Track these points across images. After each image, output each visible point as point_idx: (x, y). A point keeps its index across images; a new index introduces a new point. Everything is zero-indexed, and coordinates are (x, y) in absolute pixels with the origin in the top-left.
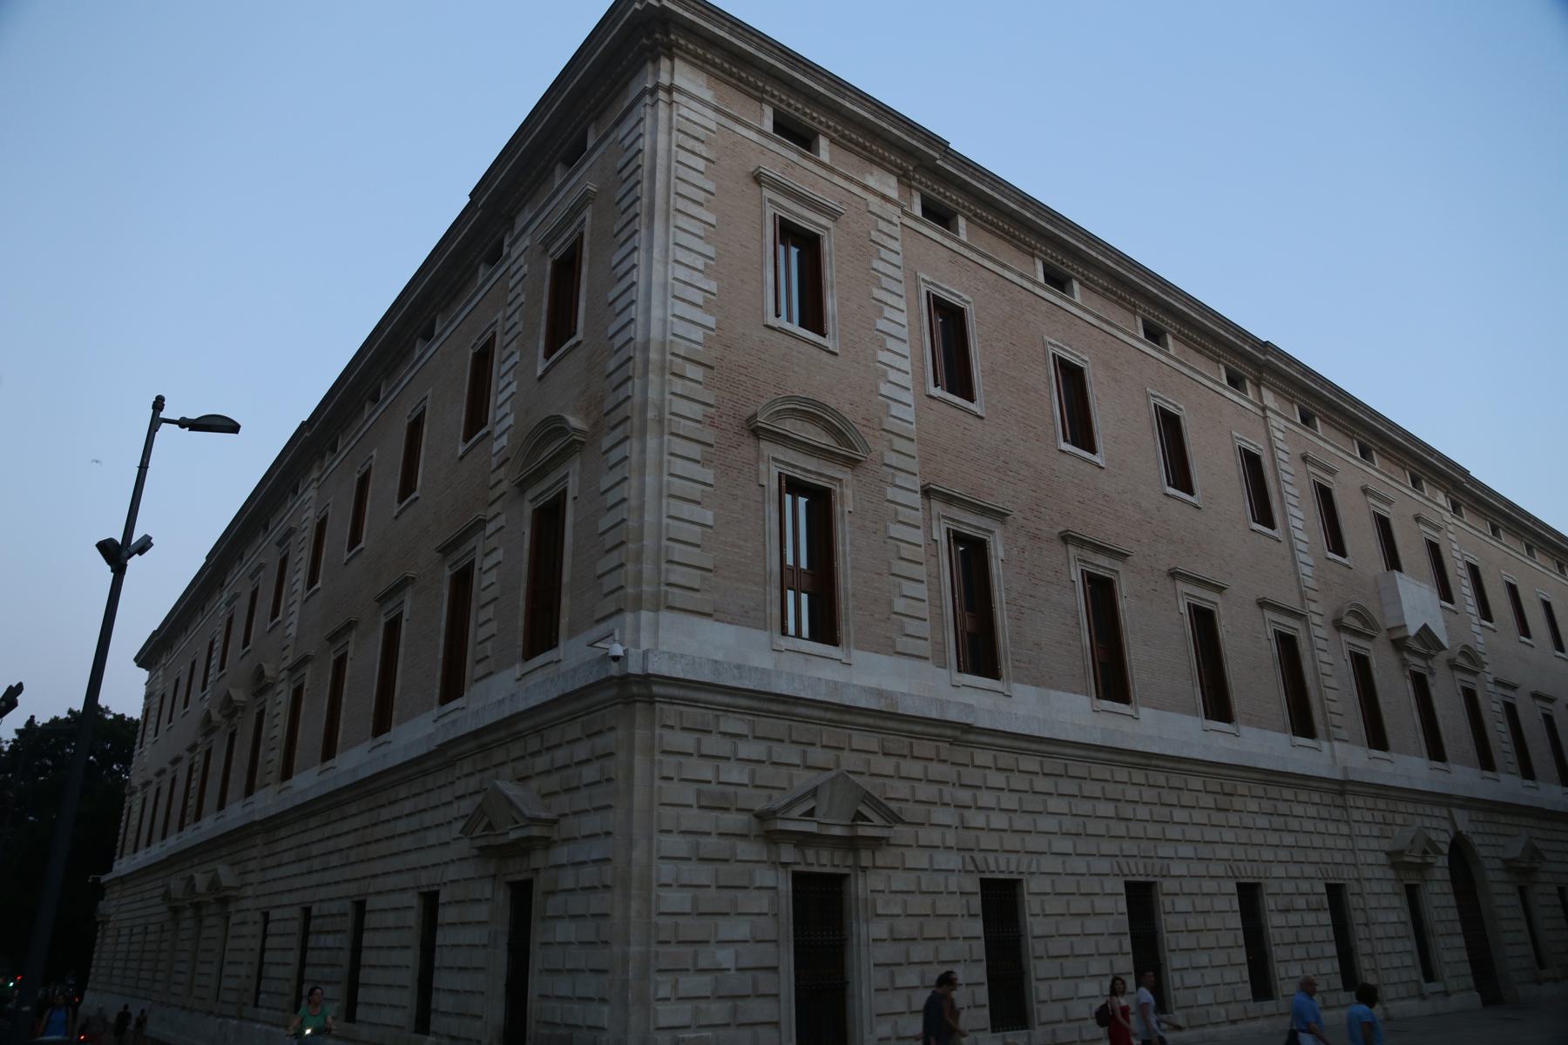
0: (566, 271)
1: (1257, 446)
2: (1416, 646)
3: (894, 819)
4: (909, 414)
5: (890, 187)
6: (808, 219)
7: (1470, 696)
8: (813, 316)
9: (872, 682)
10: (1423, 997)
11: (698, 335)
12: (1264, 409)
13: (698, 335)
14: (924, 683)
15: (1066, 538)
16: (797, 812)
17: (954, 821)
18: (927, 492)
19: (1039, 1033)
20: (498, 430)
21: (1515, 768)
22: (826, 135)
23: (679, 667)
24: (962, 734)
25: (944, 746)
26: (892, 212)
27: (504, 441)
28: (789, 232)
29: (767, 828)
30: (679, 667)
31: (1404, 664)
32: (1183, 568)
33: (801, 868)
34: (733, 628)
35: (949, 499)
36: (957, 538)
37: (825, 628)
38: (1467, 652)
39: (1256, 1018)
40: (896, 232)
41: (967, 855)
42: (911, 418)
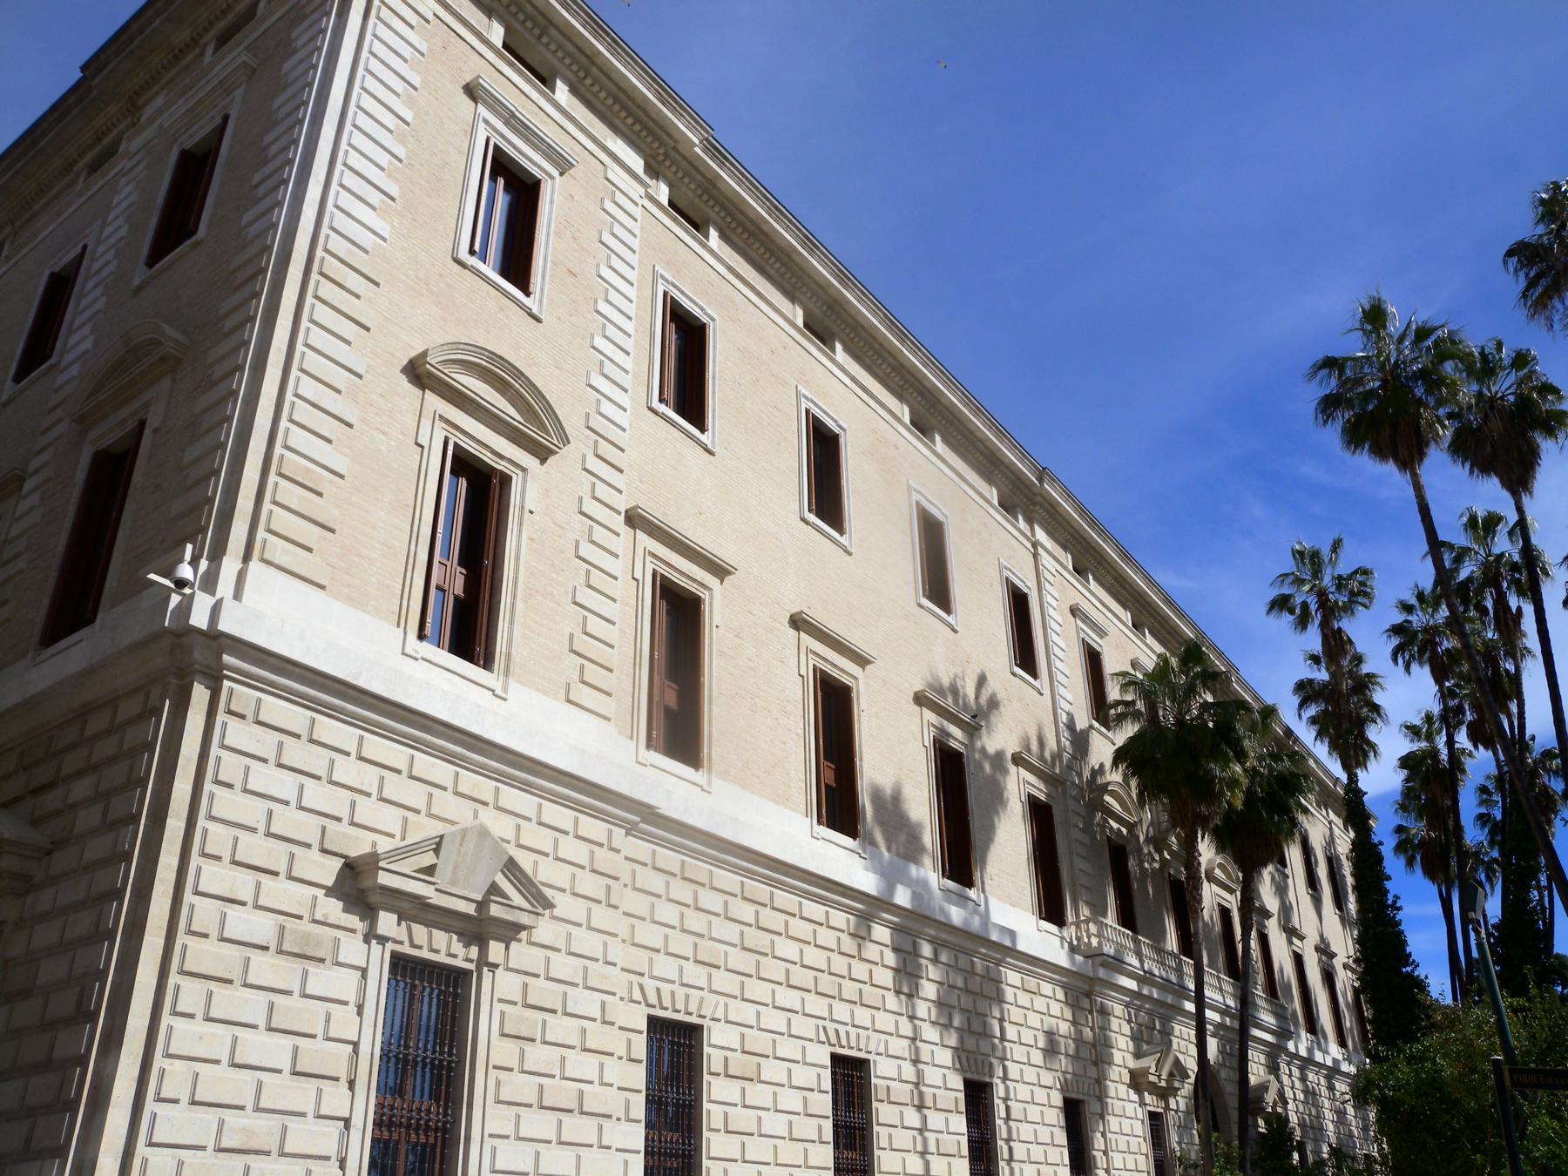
0: (194, 170)
1: (1028, 584)
6: (531, 160)
12: (1035, 545)
14: (600, 738)
16: (406, 866)
17: (624, 933)
20: (69, 358)
24: (644, 818)
25: (619, 833)
26: (636, 190)
27: (74, 371)
28: (502, 166)
29: (357, 886)
33: (407, 949)
40: (637, 212)
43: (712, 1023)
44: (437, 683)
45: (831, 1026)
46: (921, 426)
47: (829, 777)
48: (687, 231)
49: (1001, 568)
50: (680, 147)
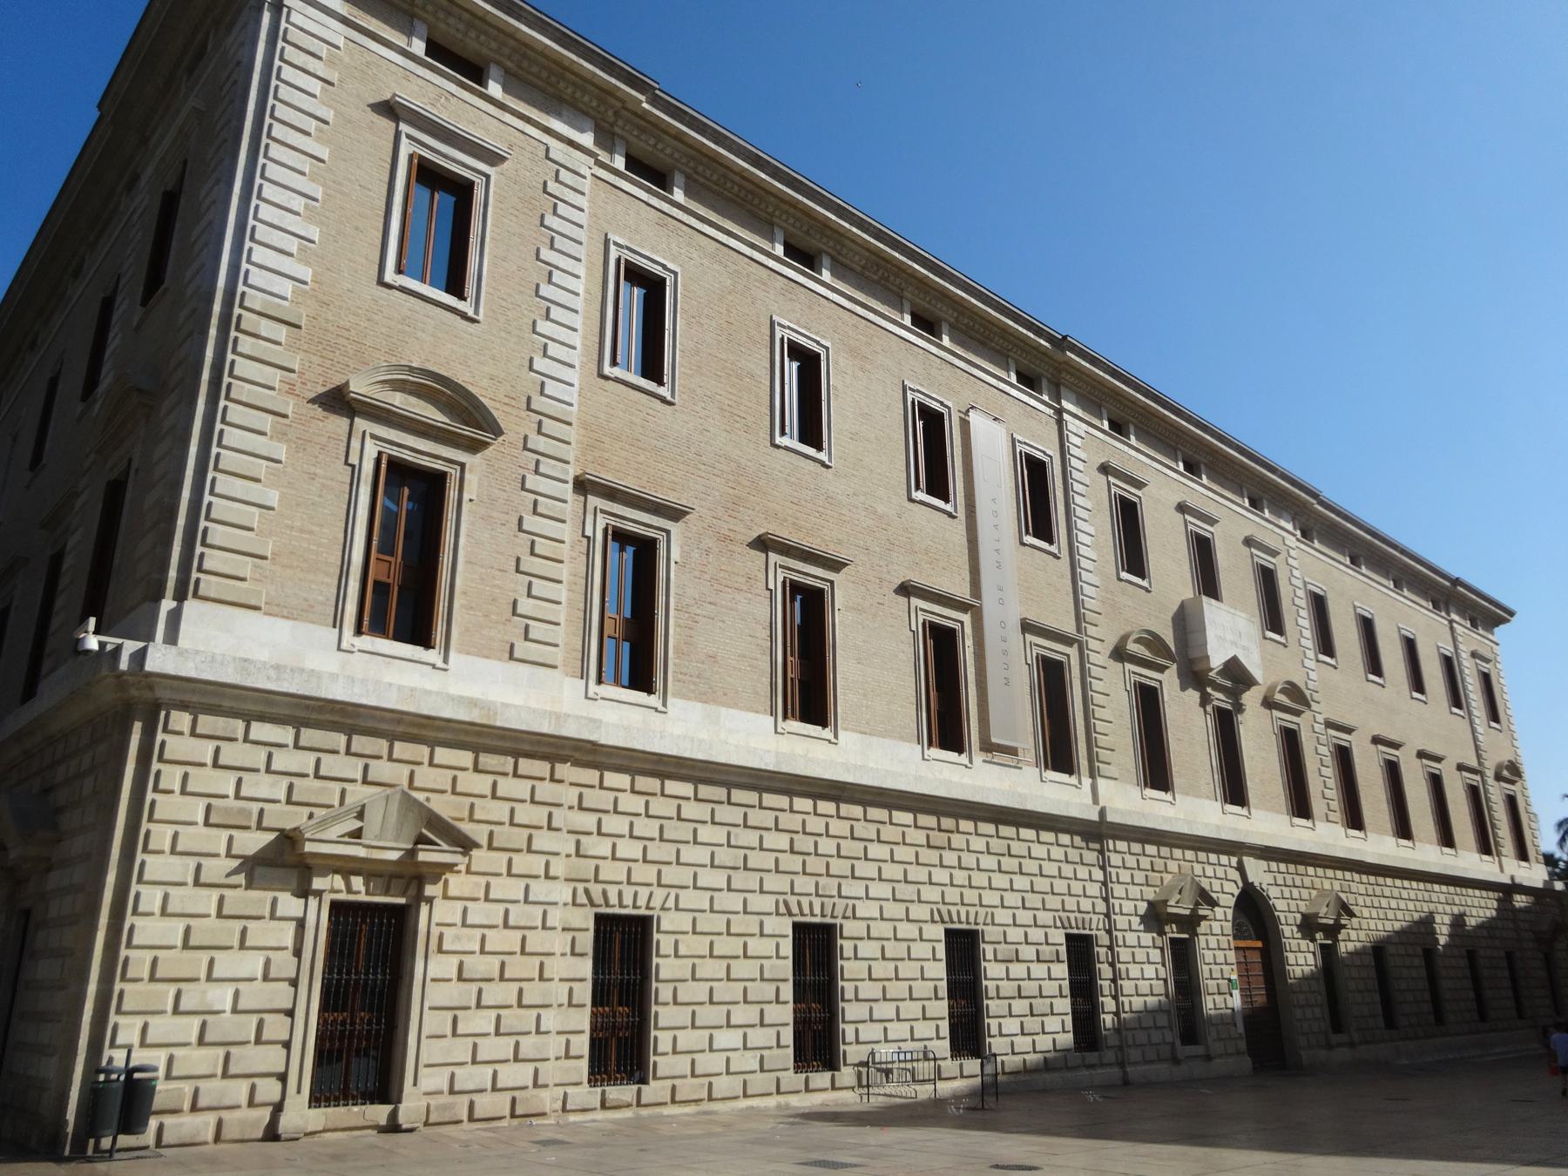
1: (1046, 448)
2: (1220, 680)
3: (466, 845)
4: (571, 394)
5: (1289, 527)
7: (1290, 742)
8: (811, 431)
9: (473, 692)
10: (1175, 1060)
11: (287, 288)
12: (1451, 622)
13: (287, 288)
15: (763, 544)
16: (335, 832)
18: (583, 486)
19: (654, 1090)
21: (1337, 816)
22: (498, 63)
23: (191, 665)
28: (427, 175)
30: (191, 665)
31: (1205, 700)
32: (920, 579)
34: (290, 623)
35: (611, 493)
36: (621, 537)
37: (641, 676)
38: (1293, 690)
39: (1077, 1068)
41: (580, 887)
42: (574, 400)
43: (662, 914)
44: (619, 718)
45: (944, 909)
46: (926, 324)
47: (389, 570)
48: (648, 191)
49: (1355, 607)
50: (630, 106)
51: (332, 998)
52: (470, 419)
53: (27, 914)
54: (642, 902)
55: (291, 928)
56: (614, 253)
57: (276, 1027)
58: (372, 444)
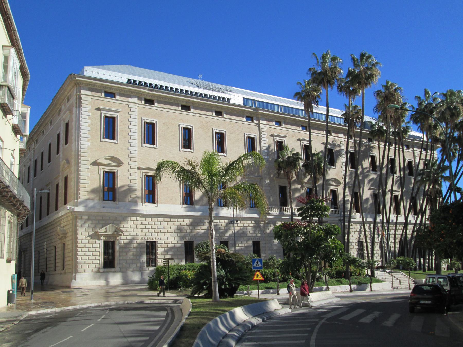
1: (254, 133)
18: (139, 168)
46: (219, 113)
51: (105, 253)
52: (117, 162)
53: (64, 244)
54: (154, 239)
55: (98, 245)
56: (246, 136)
57: (98, 258)
58: (103, 169)
